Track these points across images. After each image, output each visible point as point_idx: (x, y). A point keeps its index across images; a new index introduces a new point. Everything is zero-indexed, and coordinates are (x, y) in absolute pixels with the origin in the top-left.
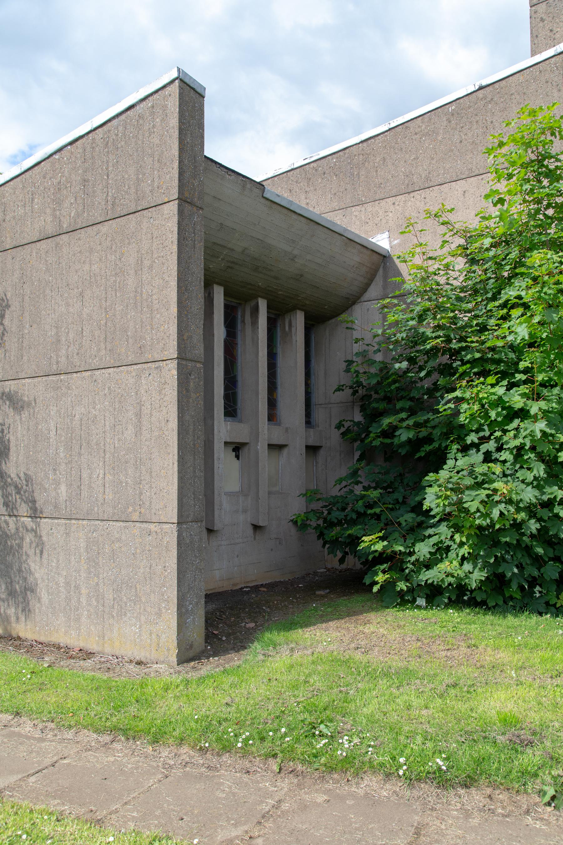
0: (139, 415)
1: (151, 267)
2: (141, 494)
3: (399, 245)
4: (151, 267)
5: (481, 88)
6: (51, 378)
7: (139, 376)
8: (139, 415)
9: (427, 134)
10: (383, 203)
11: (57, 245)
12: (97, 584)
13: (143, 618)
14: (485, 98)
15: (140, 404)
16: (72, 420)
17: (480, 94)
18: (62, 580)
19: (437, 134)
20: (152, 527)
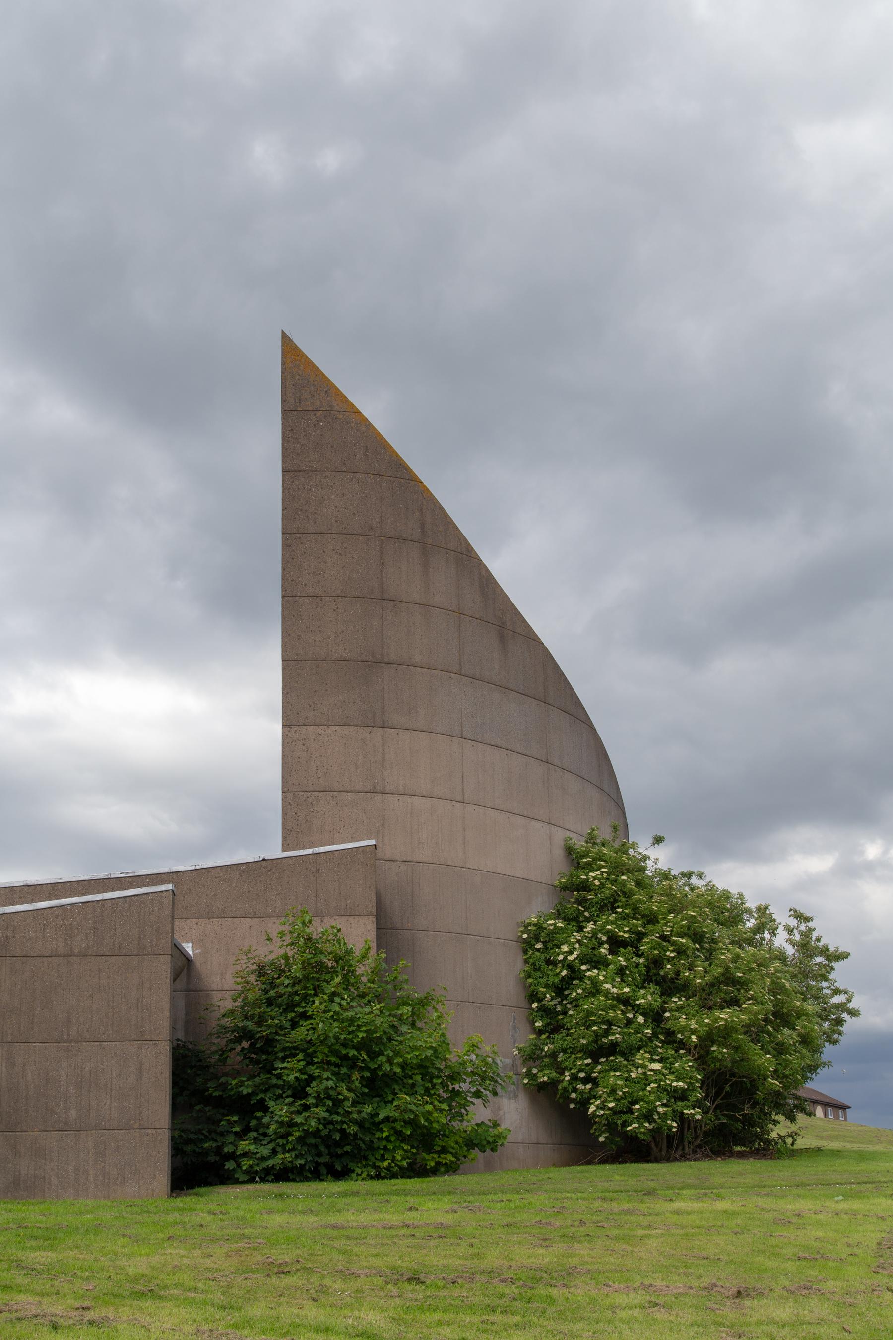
0: (140, 1070)
1: (150, 988)
2: (140, 1113)
3: (200, 954)
4: (150, 988)
5: (264, 860)
6: (61, 1044)
7: (140, 1048)
8: (140, 1070)
9: (224, 880)
10: (188, 921)
11: (69, 962)
12: (104, 1167)
13: (141, 1182)
14: (266, 867)
15: (141, 1064)
16: (82, 1071)
17: (263, 863)
18: (71, 1169)
19: (232, 882)
20: (149, 1131)
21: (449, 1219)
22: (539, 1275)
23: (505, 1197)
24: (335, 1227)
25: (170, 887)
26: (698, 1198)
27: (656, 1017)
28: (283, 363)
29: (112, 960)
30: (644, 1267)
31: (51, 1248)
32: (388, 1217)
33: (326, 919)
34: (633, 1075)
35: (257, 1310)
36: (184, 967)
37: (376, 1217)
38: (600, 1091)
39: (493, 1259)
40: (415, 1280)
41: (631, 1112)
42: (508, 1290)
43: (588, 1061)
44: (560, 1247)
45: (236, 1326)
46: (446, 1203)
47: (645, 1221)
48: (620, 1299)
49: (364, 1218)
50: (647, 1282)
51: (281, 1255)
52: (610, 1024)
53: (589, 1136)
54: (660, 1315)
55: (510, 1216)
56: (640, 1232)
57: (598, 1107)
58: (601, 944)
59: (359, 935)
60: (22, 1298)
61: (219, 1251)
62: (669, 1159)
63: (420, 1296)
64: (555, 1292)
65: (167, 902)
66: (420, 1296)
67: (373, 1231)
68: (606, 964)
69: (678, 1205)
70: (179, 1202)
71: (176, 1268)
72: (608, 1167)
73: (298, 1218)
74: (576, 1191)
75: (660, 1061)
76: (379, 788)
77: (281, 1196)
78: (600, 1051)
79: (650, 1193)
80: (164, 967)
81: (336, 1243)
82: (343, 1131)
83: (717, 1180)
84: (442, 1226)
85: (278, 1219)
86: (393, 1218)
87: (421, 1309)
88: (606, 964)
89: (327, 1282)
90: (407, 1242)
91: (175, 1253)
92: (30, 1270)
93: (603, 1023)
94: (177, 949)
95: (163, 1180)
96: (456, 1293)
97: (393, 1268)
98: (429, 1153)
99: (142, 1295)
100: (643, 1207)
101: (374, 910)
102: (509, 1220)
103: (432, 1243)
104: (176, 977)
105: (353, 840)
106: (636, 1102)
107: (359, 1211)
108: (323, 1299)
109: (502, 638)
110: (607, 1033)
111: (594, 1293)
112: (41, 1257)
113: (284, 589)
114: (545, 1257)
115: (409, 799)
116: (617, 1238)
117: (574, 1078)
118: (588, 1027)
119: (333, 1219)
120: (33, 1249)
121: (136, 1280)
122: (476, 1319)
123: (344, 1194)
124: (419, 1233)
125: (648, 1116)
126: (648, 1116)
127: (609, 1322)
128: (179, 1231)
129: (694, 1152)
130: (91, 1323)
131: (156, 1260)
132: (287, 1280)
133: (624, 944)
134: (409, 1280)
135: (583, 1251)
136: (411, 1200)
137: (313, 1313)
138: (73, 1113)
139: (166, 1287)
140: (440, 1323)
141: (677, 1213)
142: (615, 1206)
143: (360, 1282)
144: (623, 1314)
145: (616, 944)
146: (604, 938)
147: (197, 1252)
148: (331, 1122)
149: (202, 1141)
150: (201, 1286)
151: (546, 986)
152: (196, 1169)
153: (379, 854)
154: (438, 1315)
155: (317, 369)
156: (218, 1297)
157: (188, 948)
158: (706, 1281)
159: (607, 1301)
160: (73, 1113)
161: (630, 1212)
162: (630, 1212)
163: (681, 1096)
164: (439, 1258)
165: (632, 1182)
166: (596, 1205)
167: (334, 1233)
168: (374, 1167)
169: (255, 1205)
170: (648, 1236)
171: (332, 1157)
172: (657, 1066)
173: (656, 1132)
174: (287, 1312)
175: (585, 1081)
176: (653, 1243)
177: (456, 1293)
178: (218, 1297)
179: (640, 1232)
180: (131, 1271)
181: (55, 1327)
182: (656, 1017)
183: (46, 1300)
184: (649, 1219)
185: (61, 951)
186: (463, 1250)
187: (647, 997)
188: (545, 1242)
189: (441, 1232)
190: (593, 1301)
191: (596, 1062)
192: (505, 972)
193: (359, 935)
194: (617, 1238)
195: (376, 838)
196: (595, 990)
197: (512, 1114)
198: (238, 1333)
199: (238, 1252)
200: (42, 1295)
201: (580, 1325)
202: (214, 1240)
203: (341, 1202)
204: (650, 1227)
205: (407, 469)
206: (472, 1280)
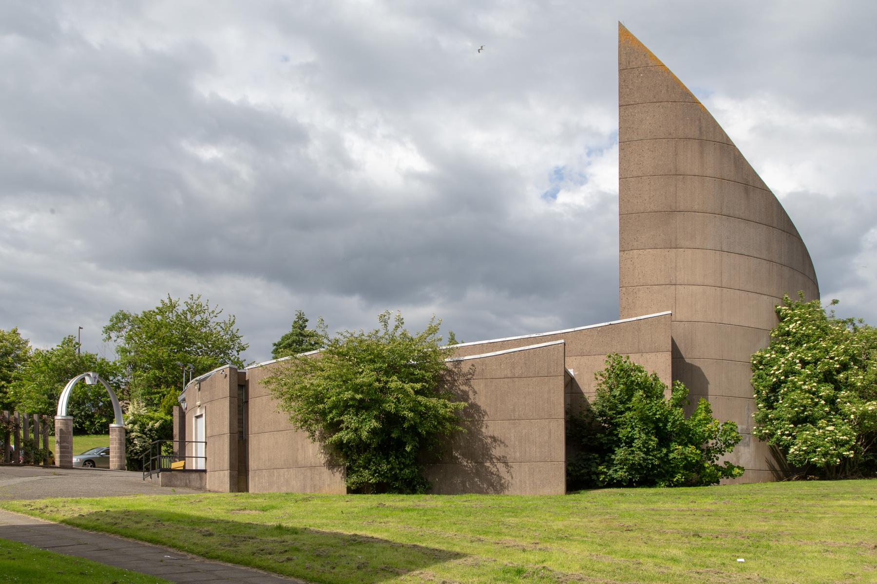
0: (550, 433)
8: (550, 433)
21: (713, 507)
22: (761, 536)
23: (742, 497)
24: (653, 510)
25: (563, 341)
26: (854, 499)
27: (831, 401)
28: (620, 41)
29: (534, 379)
30: (821, 532)
31: (516, 516)
32: (680, 505)
33: (644, 354)
34: (817, 433)
35: (619, 546)
36: (570, 384)
37: (674, 505)
38: (797, 441)
39: (737, 526)
40: (696, 535)
41: (815, 452)
42: (746, 541)
43: (792, 426)
44: (774, 522)
45: (609, 553)
46: (710, 500)
47: (822, 510)
48: (809, 548)
49: (667, 506)
50: (823, 540)
51: (628, 522)
52: (805, 406)
53: (787, 468)
54: (830, 556)
55: (745, 505)
56: (819, 516)
57: (796, 450)
58: (795, 364)
59: (657, 366)
60: (508, 538)
61: (596, 519)
62: (836, 478)
63: (700, 543)
64: (771, 544)
65: (561, 349)
66: (700, 543)
67: (673, 512)
68: (800, 373)
69: (841, 502)
70: (572, 496)
71: (577, 527)
72: (800, 482)
73: (633, 506)
74: (782, 494)
75: (833, 425)
76: (673, 282)
77: (622, 494)
78: (800, 421)
79: (825, 496)
80: (561, 382)
81: (655, 518)
82: (652, 464)
83: (865, 489)
84: (709, 510)
85: (623, 506)
86: (683, 506)
87: (700, 549)
88: (800, 373)
89: (652, 535)
90: (691, 517)
91: (575, 520)
92: (509, 526)
93: (802, 406)
94: (566, 373)
95: (562, 487)
96: (718, 542)
97: (684, 529)
98: (698, 475)
99: (562, 538)
100: (821, 503)
101: (670, 349)
102: (746, 508)
103: (704, 518)
104: (566, 386)
105: (659, 311)
106: (817, 448)
107: (664, 503)
108: (650, 542)
109: (747, 191)
110: (804, 411)
111: (793, 544)
112: (512, 520)
113: (620, 175)
114: (765, 527)
115: (691, 287)
116: (806, 518)
117: (783, 434)
118: (793, 408)
119: (652, 506)
120: (508, 517)
121: (558, 531)
122: (729, 555)
123: (655, 494)
124: (698, 513)
125: (825, 455)
126: (825, 455)
127: (801, 558)
128: (575, 510)
129: (852, 475)
130: (540, 549)
131: (566, 523)
132: (631, 534)
133: (809, 363)
134: (694, 535)
135: (787, 525)
136: (692, 498)
137: (645, 549)
138: (518, 454)
139: (572, 535)
140: (710, 556)
141: (842, 506)
142: (804, 502)
143: (667, 536)
144: (809, 555)
145: (804, 363)
146: (798, 361)
147: (585, 520)
148: (647, 459)
149: (580, 470)
150: (589, 535)
151: (764, 387)
152: (578, 480)
153: (673, 319)
154: (709, 553)
155: (639, 42)
156: (598, 540)
157: (571, 371)
158: (857, 541)
159: (800, 549)
160: (518, 454)
161: (813, 506)
162: (813, 506)
163: (842, 444)
164: (709, 525)
165: (814, 490)
166: (794, 501)
167: (653, 512)
168: (669, 481)
169: (612, 498)
170: (824, 518)
171: (646, 477)
172: (831, 428)
173: (827, 464)
174: (633, 549)
175: (788, 435)
176: (826, 521)
177: (718, 542)
178: (598, 540)
179: (819, 516)
180: (555, 528)
181: (524, 550)
182: (831, 401)
183: (517, 539)
184: (825, 509)
185: (509, 375)
186: (721, 522)
187: (826, 390)
188: (766, 519)
189: (710, 513)
190: (793, 548)
191: (796, 425)
192: (743, 381)
193: (657, 366)
194: (806, 518)
195: (671, 309)
196: (796, 387)
197: (745, 455)
198: (610, 557)
199: (606, 520)
200: (515, 537)
201: (785, 559)
202: (593, 515)
203: (655, 498)
204: (824, 513)
205: (692, 96)
206: (726, 536)
